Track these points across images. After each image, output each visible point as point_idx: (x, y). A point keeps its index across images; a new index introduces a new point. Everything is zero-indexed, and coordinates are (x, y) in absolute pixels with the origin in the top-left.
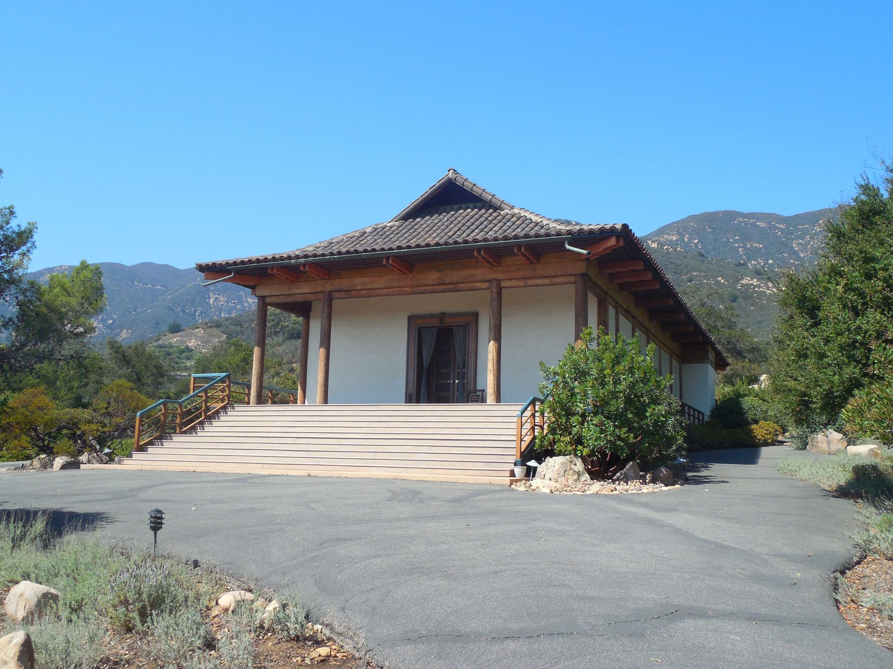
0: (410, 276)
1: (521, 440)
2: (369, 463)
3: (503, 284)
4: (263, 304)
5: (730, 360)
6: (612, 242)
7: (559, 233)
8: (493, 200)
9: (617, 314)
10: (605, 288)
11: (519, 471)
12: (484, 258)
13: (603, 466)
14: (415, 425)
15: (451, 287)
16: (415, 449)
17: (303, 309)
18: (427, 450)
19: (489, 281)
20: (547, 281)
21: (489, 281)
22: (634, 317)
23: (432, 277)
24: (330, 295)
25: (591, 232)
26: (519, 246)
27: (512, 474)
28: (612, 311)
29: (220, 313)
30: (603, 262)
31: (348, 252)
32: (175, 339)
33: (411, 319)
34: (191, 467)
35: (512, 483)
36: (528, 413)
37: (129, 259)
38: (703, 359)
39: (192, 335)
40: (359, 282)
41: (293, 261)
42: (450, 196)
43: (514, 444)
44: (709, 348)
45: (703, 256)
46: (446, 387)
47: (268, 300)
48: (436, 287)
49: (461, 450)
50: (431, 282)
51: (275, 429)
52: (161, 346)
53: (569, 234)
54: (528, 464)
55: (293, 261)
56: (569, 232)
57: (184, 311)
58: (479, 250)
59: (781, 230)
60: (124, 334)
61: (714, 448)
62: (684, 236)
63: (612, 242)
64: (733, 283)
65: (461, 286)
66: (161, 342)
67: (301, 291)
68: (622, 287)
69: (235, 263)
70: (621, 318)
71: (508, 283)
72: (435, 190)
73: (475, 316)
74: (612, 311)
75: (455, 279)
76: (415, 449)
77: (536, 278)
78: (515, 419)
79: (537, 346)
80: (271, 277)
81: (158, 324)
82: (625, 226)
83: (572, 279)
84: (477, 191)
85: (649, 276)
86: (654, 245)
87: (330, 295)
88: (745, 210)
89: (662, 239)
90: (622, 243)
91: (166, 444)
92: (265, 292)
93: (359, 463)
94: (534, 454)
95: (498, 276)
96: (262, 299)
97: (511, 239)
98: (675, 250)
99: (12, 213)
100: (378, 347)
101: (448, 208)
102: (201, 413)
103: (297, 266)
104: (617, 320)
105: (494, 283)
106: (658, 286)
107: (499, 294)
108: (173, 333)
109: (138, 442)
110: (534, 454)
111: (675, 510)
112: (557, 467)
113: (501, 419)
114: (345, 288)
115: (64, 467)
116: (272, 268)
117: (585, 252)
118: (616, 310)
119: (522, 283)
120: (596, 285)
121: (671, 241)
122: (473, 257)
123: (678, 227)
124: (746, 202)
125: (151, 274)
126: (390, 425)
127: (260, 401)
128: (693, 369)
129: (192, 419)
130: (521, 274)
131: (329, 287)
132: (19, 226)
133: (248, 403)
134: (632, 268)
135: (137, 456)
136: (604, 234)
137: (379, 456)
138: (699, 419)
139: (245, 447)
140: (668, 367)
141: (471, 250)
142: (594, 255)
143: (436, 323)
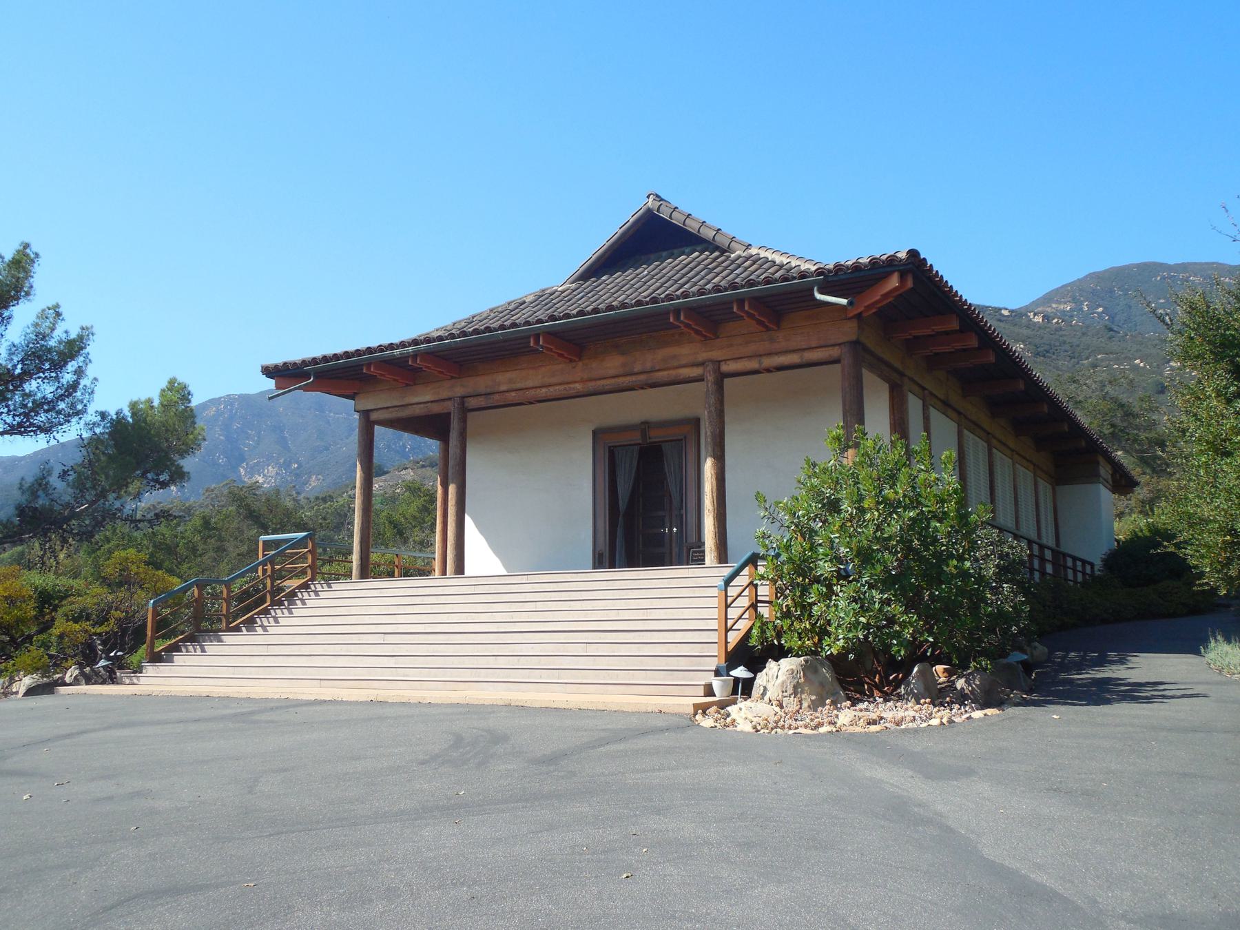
1: (727, 631)
2: (483, 675)
5: (1143, 479)
7: (803, 275)
10: (897, 365)
12: (687, 326)
13: (859, 673)
14: (578, 605)
15: (642, 377)
16: (561, 650)
17: (432, 425)
19: (702, 364)
21: (702, 364)
22: (959, 413)
23: (612, 364)
24: (463, 403)
25: (857, 267)
26: (741, 301)
27: (709, 691)
28: (914, 405)
30: (890, 318)
33: (598, 435)
36: (742, 580)
38: (1093, 477)
40: (504, 380)
41: (396, 352)
42: (653, 236)
44: (1101, 459)
45: (1111, 330)
46: (659, 540)
47: (374, 416)
48: (621, 380)
49: (634, 650)
50: (612, 372)
51: (367, 620)
54: (732, 673)
55: (396, 352)
57: (389, 447)
58: (677, 311)
60: (314, 482)
63: (894, 282)
67: (422, 398)
68: (933, 363)
69: (314, 361)
70: (933, 413)
72: (629, 229)
73: (696, 422)
74: (914, 405)
75: (648, 366)
77: (777, 354)
78: (715, 592)
79: (776, 469)
82: (913, 254)
84: (692, 226)
85: (974, 342)
86: (1039, 319)
87: (463, 403)
88: (1171, 262)
89: (1049, 310)
90: (910, 283)
91: (211, 648)
92: (369, 405)
93: (467, 675)
94: (750, 655)
95: (716, 354)
96: (365, 414)
97: (726, 289)
99: (58, 314)
100: (557, 482)
102: (265, 595)
105: (710, 367)
106: (992, 359)
110: (750, 655)
111: (969, 773)
112: (782, 678)
115: (30, 692)
117: (844, 301)
120: (880, 359)
121: (1063, 311)
126: (540, 606)
127: (365, 573)
128: (1073, 494)
129: (252, 605)
130: (752, 348)
131: (459, 391)
132: (66, 332)
134: (938, 328)
135: (150, 670)
136: (879, 269)
137: (502, 662)
138: (1084, 573)
139: (332, 649)
140: (985, 494)
141: (665, 313)
143: (636, 438)
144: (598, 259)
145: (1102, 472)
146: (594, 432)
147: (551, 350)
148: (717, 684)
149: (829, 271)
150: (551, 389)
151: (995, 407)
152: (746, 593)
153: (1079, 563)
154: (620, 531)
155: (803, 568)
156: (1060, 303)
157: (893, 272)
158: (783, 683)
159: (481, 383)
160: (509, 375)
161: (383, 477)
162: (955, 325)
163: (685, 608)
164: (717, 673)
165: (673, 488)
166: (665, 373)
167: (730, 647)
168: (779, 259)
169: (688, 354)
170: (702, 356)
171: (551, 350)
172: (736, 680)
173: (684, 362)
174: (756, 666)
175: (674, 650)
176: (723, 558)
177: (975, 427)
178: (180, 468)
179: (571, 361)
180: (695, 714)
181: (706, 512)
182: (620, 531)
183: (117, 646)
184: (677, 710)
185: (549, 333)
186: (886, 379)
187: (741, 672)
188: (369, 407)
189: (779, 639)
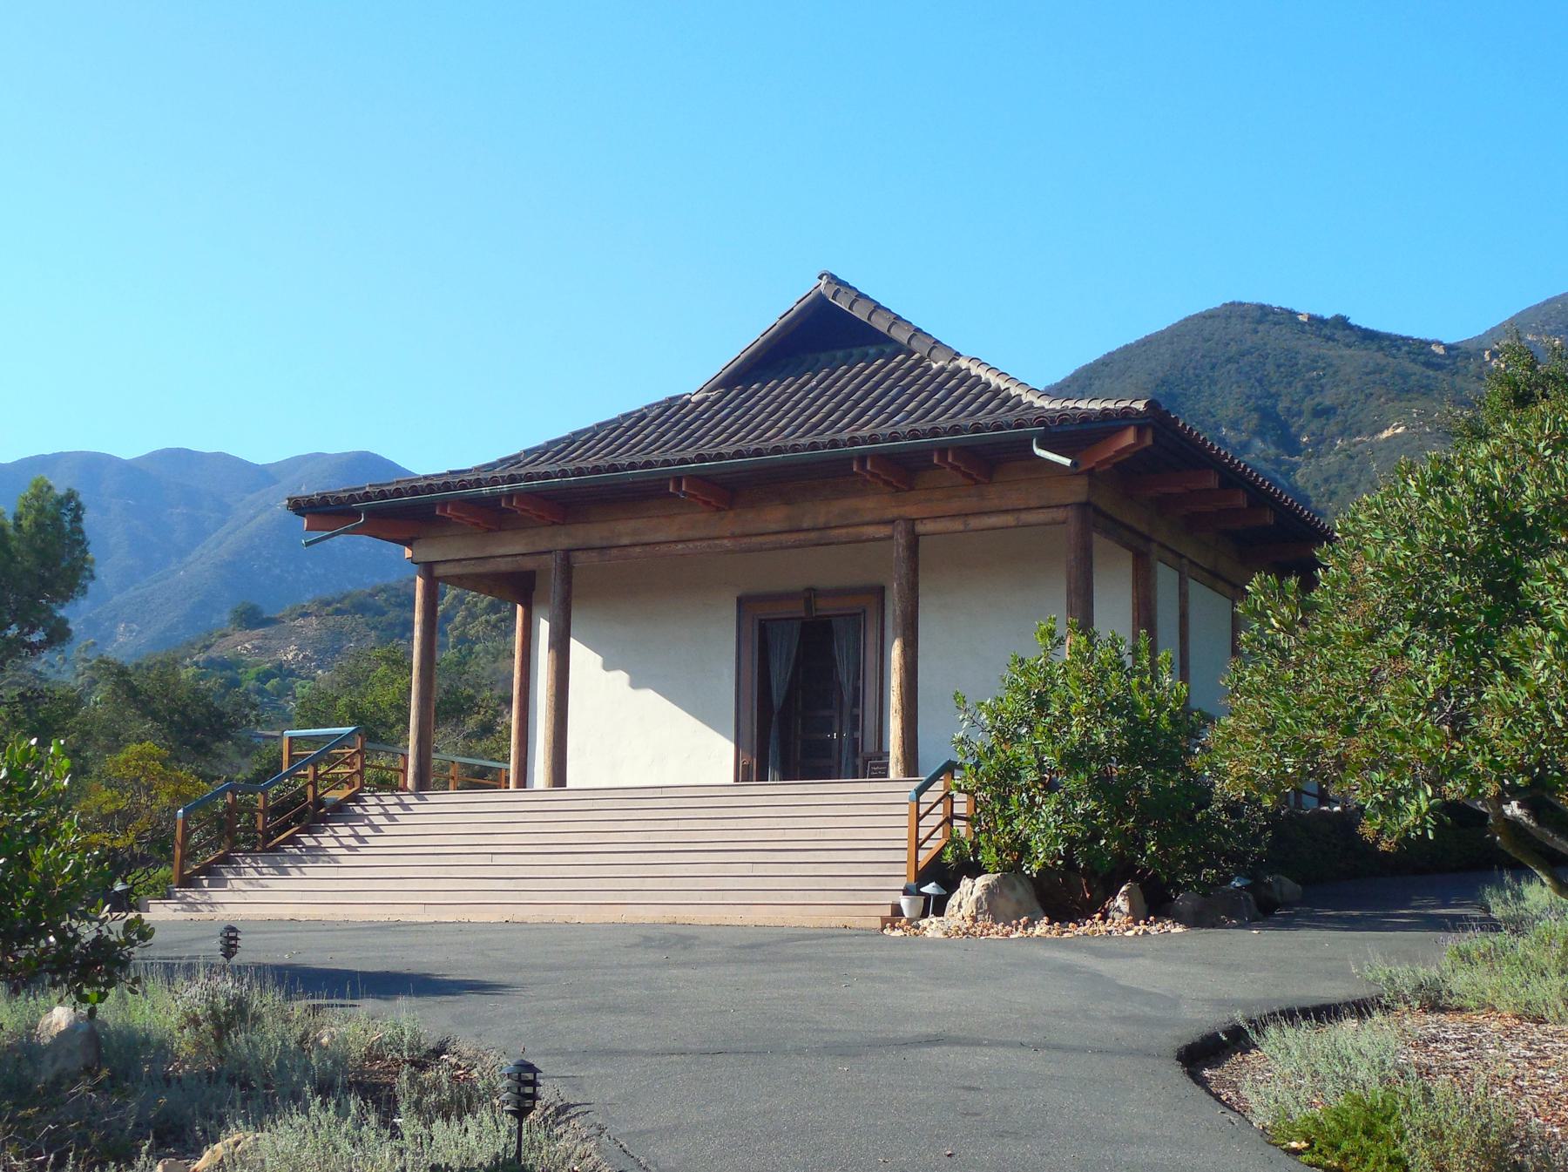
0: (731, 514)
3: (920, 528)
6: (1129, 438)
9: (1182, 583)
12: (873, 475)
13: (1064, 895)
15: (813, 535)
16: (722, 870)
18: (744, 869)
19: (892, 522)
20: (1009, 519)
23: (774, 517)
30: (1129, 475)
33: (741, 602)
34: (287, 912)
36: (939, 786)
37: (129, 445)
40: (625, 530)
42: (826, 334)
43: (903, 856)
47: (440, 571)
48: (783, 537)
50: (774, 527)
53: (1041, 424)
54: (923, 890)
55: (485, 490)
63: (1129, 438)
66: (213, 653)
67: (509, 549)
70: (1196, 590)
73: (880, 592)
74: (1166, 579)
75: (821, 521)
76: (722, 870)
79: (978, 662)
80: (444, 522)
83: (1059, 514)
85: (1241, 501)
90: (1148, 441)
94: (942, 874)
95: (910, 511)
103: (495, 499)
104: (1183, 596)
105: (901, 527)
109: (182, 871)
110: (942, 874)
114: (598, 543)
117: (1067, 462)
118: (1181, 573)
119: (957, 525)
125: (181, 485)
126: (683, 825)
129: (289, 821)
130: (955, 505)
141: (847, 461)
143: (798, 609)
146: (739, 600)
148: (904, 902)
149: (1053, 421)
150: (691, 545)
154: (774, 733)
155: (1008, 774)
157: (1126, 427)
158: (978, 899)
159: (595, 533)
161: (261, 631)
162: (1213, 482)
163: (862, 828)
164: (906, 892)
165: (844, 676)
166: (844, 531)
167: (920, 866)
168: (996, 381)
169: (872, 508)
172: (927, 897)
173: (868, 518)
174: (950, 886)
175: (855, 870)
176: (911, 768)
178: (63, 622)
180: (884, 928)
181: (892, 711)
182: (774, 733)
185: (697, 477)
186: (1127, 546)
188: (431, 559)
189: (975, 857)
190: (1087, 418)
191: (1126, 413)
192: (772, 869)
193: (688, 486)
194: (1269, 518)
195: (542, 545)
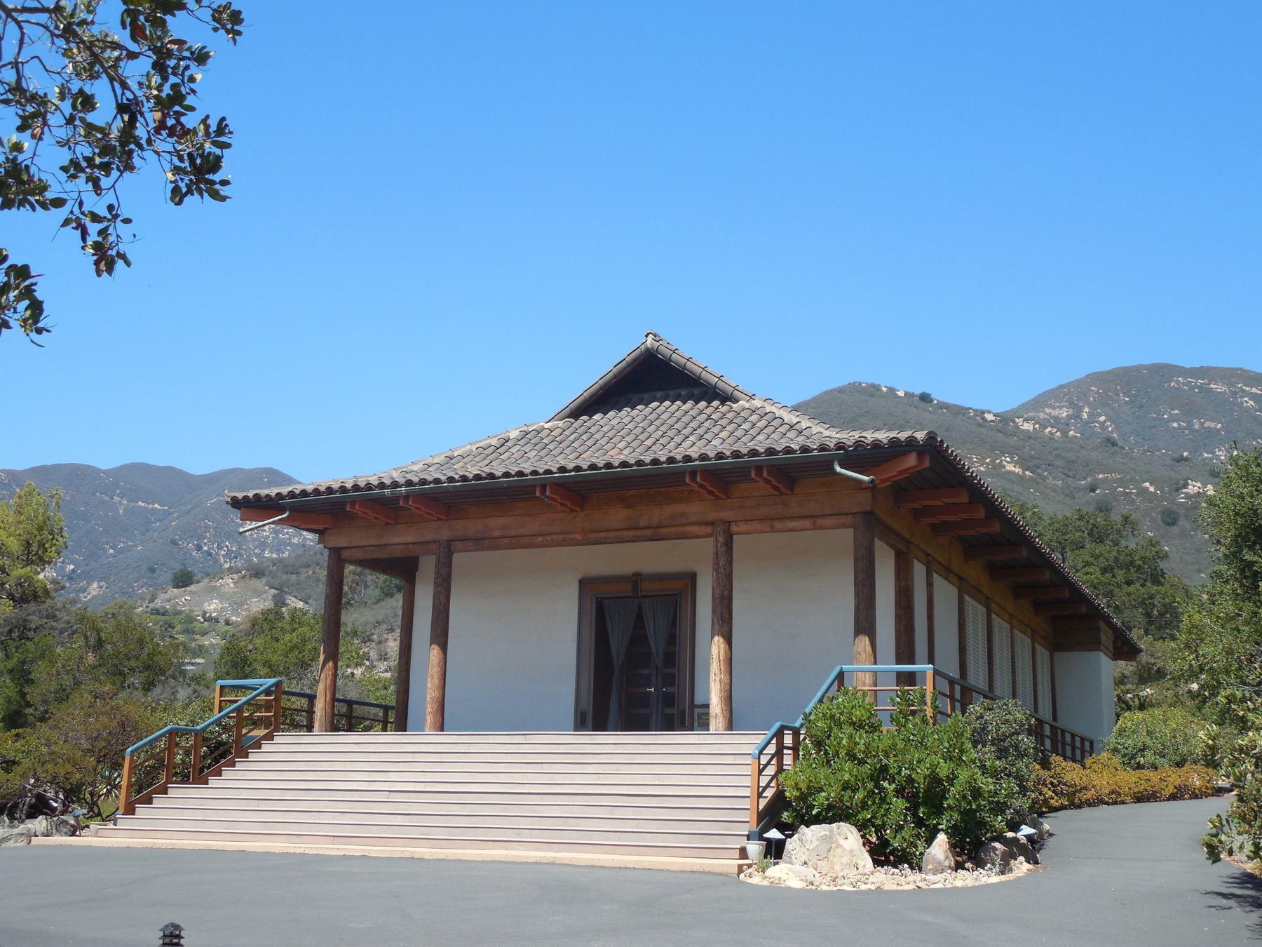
0: (582, 514)
1: (760, 795)
3: (734, 528)
4: (338, 560)
7: (823, 448)
8: (720, 384)
9: (929, 574)
11: (754, 848)
12: (701, 486)
15: (648, 532)
17: (402, 569)
19: (712, 523)
22: (960, 578)
23: (617, 516)
27: (743, 853)
28: (919, 570)
29: (263, 551)
30: (901, 491)
31: (477, 477)
32: (181, 599)
35: (740, 869)
38: (1094, 645)
39: (212, 591)
40: (497, 524)
42: (650, 377)
43: (746, 804)
44: (1102, 625)
45: (1114, 444)
47: (346, 554)
48: (625, 533)
52: (156, 612)
56: (840, 446)
58: (693, 473)
59: (1253, 397)
60: (94, 589)
61: (1090, 805)
62: (1080, 410)
63: (911, 461)
64: (1170, 492)
65: (665, 531)
67: (401, 539)
70: (938, 580)
71: (743, 527)
73: (692, 577)
74: (919, 570)
81: (152, 570)
83: (849, 519)
85: (981, 513)
86: (1028, 427)
87: (449, 547)
88: (1188, 364)
90: (927, 464)
92: (341, 542)
94: (781, 817)
95: (726, 515)
98: (1065, 434)
101: (646, 396)
103: (395, 499)
104: (930, 585)
107: (729, 544)
108: (178, 587)
110: (781, 817)
113: (730, 760)
116: (353, 503)
121: (1057, 418)
122: (684, 483)
123: (1071, 393)
124: (1187, 354)
129: (214, 755)
131: (445, 534)
133: (310, 728)
139: (304, 800)
142: (883, 481)
144: (591, 396)
145: (1103, 637)
147: (555, 500)
151: (996, 571)
152: (774, 762)
153: (1078, 739)
156: (1054, 408)
160: (502, 521)
162: (965, 499)
163: (710, 769)
166: (673, 529)
167: (761, 807)
170: (712, 515)
171: (555, 500)
172: (769, 840)
174: (789, 829)
177: (976, 593)
179: (572, 510)
183: (72, 797)
184: (721, 870)
185: (556, 484)
187: (774, 834)
190: (876, 445)
191: (911, 441)
192: (629, 814)
193: (552, 492)
194: (997, 528)
195: (429, 536)
